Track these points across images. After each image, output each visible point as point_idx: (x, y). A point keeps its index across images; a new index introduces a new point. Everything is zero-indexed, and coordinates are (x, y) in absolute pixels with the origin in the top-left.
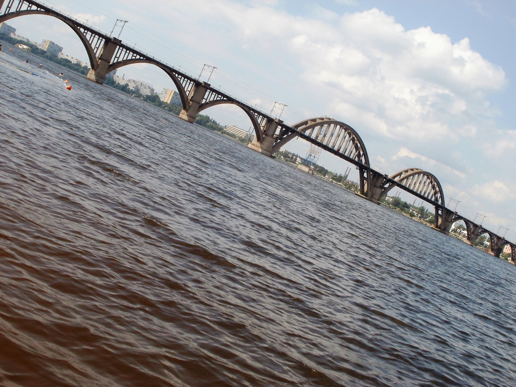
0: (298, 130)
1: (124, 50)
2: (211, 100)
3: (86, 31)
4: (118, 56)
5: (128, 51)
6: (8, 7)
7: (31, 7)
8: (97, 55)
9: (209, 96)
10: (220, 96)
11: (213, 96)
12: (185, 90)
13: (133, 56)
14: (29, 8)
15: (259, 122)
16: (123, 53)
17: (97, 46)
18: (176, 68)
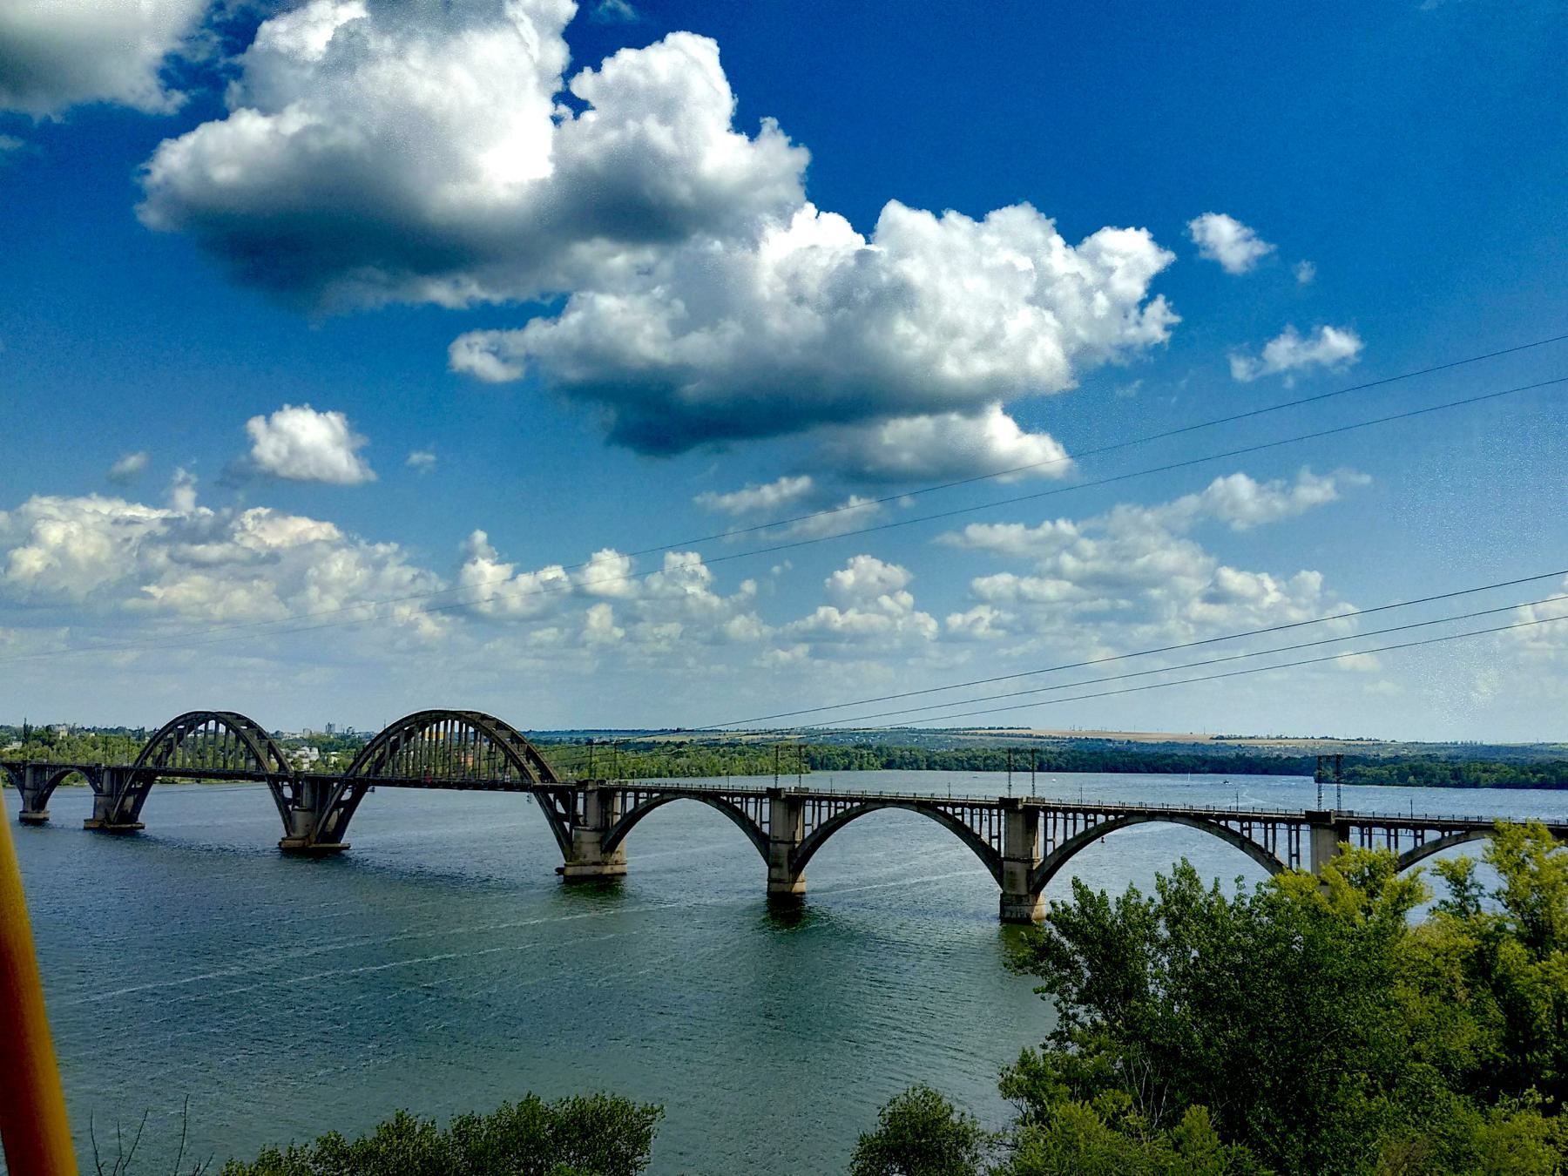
3: (1246, 825)
5: (1070, 815)
6: (1297, 855)
7: (1422, 837)
10: (840, 804)
11: (825, 811)
13: (1087, 821)
16: (1060, 822)
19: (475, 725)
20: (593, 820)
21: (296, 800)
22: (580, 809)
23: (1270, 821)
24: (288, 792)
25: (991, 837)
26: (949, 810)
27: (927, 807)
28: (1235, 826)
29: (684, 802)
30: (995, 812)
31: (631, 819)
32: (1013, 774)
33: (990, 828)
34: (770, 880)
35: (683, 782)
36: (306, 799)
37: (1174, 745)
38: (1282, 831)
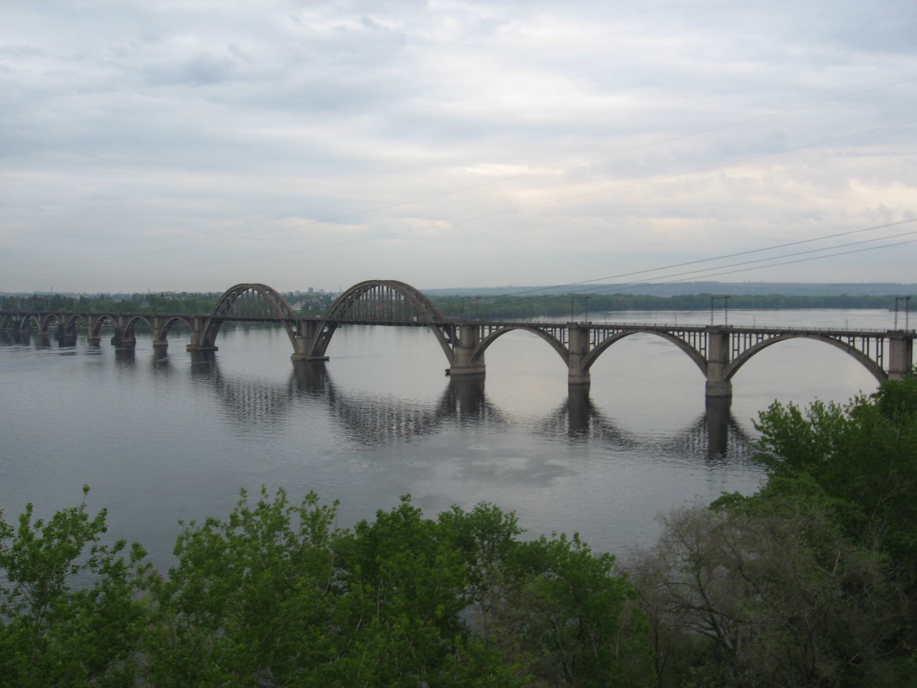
3: (851, 339)
4: (736, 348)
5: (748, 335)
6: (882, 356)
10: (611, 331)
12: (698, 348)
13: (758, 338)
15: (558, 338)
16: (742, 339)
19: (395, 288)
20: (465, 343)
23: (866, 336)
24: (295, 329)
25: (701, 349)
26: (676, 334)
27: (663, 331)
28: (845, 339)
29: (640, 335)
30: (703, 334)
31: (601, 349)
33: (701, 343)
35: (520, 321)
37: (648, 285)
38: (873, 341)
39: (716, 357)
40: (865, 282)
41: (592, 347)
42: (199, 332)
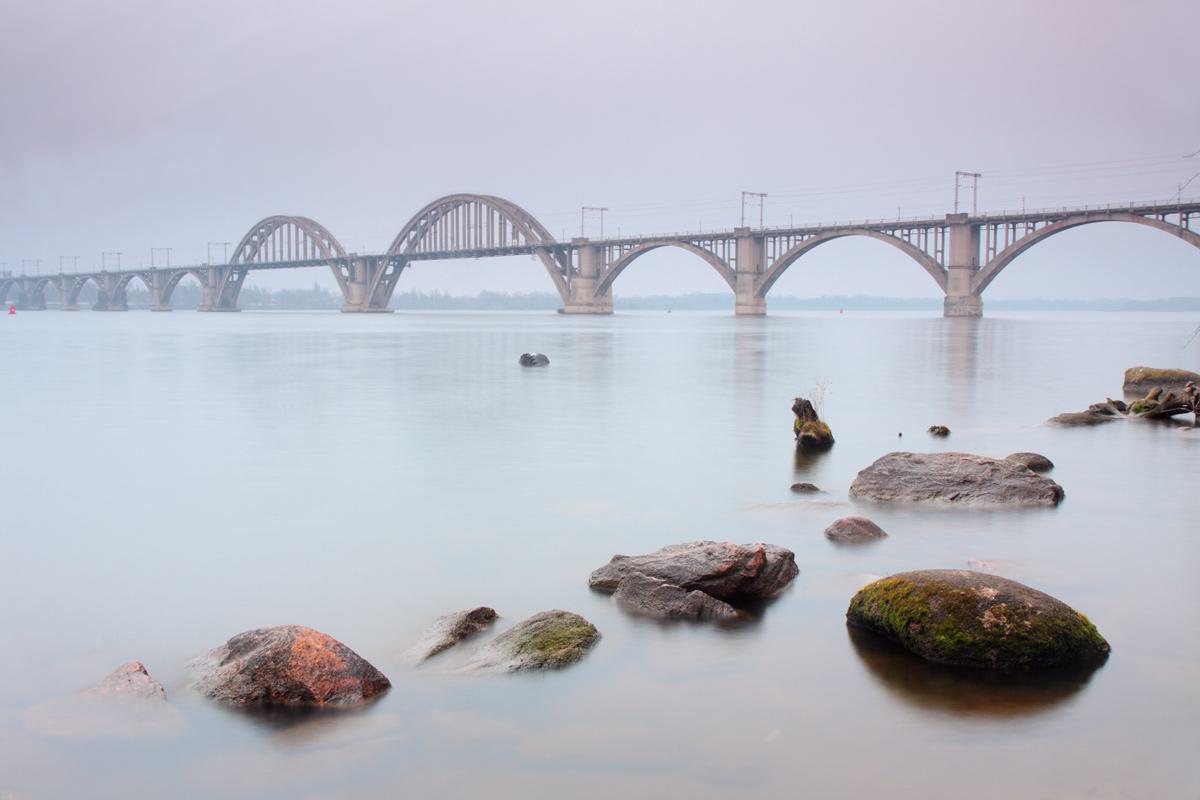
0: (402, 252)
1: (785, 238)
2: (1000, 248)
4: (992, 245)
8: (947, 264)
9: (775, 250)
13: (796, 240)
14: (1030, 231)
17: (939, 248)
18: (695, 231)
19: (500, 209)
20: (586, 270)
21: (352, 279)
22: (575, 264)
25: (936, 251)
32: (740, 227)
34: (737, 304)
36: (359, 276)
39: (963, 260)
40: (292, 269)
41: (770, 263)
42: (215, 287)
